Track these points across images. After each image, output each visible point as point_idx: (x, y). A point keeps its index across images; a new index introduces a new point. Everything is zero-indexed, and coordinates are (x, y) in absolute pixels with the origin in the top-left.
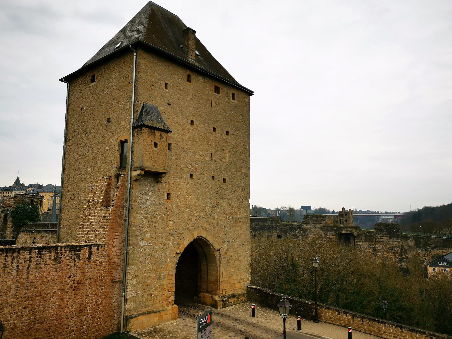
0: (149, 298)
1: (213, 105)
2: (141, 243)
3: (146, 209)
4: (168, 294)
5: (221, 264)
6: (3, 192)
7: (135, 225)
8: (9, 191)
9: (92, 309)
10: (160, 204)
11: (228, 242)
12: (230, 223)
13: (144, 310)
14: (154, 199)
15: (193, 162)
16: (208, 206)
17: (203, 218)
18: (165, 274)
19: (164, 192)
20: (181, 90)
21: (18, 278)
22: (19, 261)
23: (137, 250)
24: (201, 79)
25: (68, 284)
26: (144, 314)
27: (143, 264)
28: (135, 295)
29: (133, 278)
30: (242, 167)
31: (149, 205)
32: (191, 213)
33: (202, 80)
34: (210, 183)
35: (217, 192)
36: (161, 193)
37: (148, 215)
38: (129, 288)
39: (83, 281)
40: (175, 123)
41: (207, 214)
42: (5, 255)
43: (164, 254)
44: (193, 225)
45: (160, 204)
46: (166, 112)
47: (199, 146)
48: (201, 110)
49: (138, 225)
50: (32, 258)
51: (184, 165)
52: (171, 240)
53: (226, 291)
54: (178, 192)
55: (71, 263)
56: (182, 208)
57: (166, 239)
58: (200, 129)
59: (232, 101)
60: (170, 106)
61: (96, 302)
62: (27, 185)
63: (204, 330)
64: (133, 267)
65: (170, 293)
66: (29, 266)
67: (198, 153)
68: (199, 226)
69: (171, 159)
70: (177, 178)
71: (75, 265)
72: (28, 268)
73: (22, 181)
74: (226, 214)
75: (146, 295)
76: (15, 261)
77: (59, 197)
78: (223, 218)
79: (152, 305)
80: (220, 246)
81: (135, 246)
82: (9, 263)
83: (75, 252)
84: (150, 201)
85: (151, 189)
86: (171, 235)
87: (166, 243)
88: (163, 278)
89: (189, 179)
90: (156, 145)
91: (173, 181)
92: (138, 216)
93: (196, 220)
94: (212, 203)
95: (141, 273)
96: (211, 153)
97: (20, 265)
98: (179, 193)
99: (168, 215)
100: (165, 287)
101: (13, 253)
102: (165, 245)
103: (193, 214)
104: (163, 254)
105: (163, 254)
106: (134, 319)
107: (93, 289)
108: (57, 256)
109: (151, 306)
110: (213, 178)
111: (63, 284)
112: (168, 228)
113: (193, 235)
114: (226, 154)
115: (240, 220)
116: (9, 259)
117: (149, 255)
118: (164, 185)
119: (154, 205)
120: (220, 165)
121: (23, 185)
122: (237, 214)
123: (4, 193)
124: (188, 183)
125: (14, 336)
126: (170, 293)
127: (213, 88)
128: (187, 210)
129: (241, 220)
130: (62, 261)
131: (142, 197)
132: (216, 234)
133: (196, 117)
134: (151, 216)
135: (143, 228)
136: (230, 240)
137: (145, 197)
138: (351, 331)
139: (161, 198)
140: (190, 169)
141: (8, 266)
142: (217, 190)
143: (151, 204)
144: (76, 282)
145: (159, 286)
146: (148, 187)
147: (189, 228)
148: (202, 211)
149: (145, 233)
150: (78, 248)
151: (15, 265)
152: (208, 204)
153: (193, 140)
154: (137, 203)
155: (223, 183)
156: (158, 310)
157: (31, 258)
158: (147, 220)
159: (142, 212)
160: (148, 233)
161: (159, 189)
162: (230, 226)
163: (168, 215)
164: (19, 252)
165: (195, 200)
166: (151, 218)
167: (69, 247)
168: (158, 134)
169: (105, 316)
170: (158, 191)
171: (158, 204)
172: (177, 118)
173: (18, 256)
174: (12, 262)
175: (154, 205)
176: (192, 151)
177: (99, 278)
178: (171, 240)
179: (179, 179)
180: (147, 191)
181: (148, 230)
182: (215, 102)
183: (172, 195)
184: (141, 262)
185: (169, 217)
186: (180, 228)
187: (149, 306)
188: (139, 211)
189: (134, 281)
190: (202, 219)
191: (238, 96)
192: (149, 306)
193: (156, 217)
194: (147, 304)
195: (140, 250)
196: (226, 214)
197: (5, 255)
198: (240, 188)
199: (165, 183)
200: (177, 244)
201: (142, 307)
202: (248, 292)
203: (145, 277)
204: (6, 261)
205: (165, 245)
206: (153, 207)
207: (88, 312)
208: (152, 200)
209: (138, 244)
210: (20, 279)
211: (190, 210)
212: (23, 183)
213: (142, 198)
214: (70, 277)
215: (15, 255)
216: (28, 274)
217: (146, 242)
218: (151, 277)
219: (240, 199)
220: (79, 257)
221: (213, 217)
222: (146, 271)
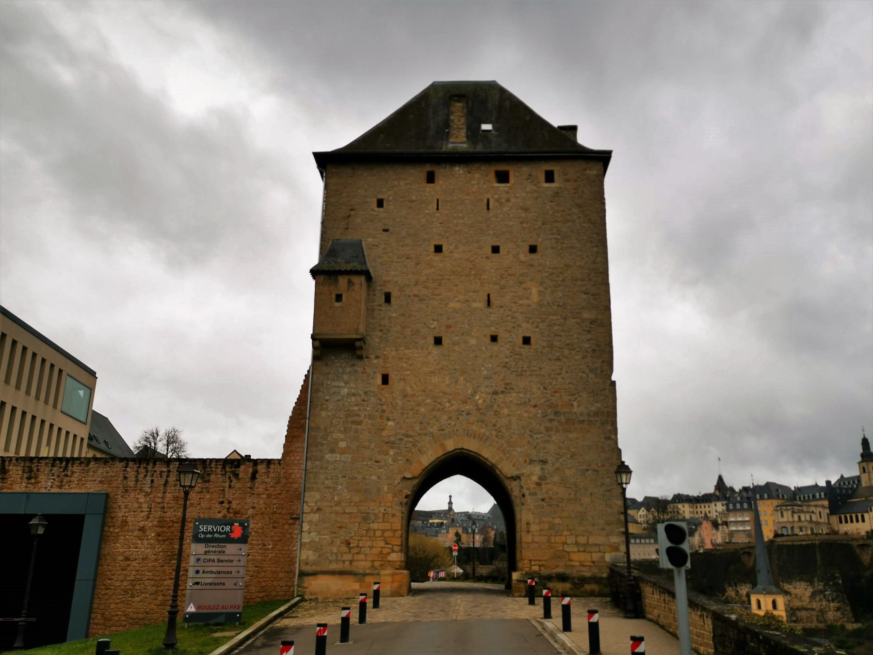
0: (344, 548)
1: (491, 207)
2: (328, 456)
3: (339, 403)
4: (385, 547)
5: (523, 507)
6: (695, 506)
7: (318, 428)
8: (701, 503)
9: (257, 555)
10: (366, 393)
11: (544, 462)
12: (549, 425)
13: (334, 567)
14: (354, 386)
15: (441, 315)
16: (482, 393)
17: (468, 414)
18: (377, 512)
19: (375, 373)
20: (412, 201)
21: (152, 496)
22: (153, 474)
23: (322, 468)
25: (219, 512)
26: (333, 573)
27: (331, 491)
28: (317, 540)
29: (312, 511)
30: (583, 308)
31: (344, 396)
32: (439, 406)
33: (461, 172)
34: (486, 349)
35: (504, 364)
36: (369, 375)
37: (342, 411)
38: (306, 527)
39: (242, 511)
40: (398, 258)
41: (480, 407)
42: (138, 465)
43: (376, 477)
44: (444, 427)
45: (366, 393)
46: (379, 243)
47: (456, 286)
48: (461, 221)
49: (322, 427)
50: (170, 471)
51: (420, 323)
52: (391, 453)
53: (543, 565)
54: (407, 370)
55: (225, 482)
56: (415, 399)
57: (379, 452)
58: (456, 255)
60: (388, 233)
61: (264, 545)
62: (737, 488)
63: (217, 544)
64: (312, 493)
65: (391, 546)
66: (167, 482)
67: (454, 297)
68: (457, 430)
69: (390, 318)
70: (402, 348)
71: (230, 486)
72: (165, 485)
73: (728, 482)
74: (535, 406)
75: (338, 542)
76: (149, 474)
77: (789, 508)
78: (526, 415)
79: (351, 562)
80: (518, 469)
81: (317, 461)
82: (141, 476)
83: (231, 468)
84: (346, 390)
85: (348, 369)
86: (392, 444)
87: (379, 458)
88: (373, 518)
89: (431, 347)
91: (394, 353)
92: (324, 414)
93: (450, 418)
94: (492, 386)
95: (328, 504)
96: (489, 295)
97: (155, 480)
98: (409, 373)
99: (383, 411)
100: (378, 533)
101: (148, 464)
102: (377, 462)
103: (443, 409)
104: (374, 478)
105: (374, 478)
106: (311, 578)
107: (260, 524)
108: (205, 472)
109: (347, 563)
110: (494, 339)
111: (212, 511)
112: (385, 433)
113: (443, 446)
114: (530, 289)
115: (581, 418)
116: (142, 470)
117: (344, 477)
118: (376, 361)
119: (354, 395)
120: (514, 312)
121: (732, 489)
122: (572, 405)
123: (697, 507)
124: (430, 353)
125: (144, 569)
126: (391, 546)
127: (492, 176)
128: (428, 401)
129: (586, 418)
130: (211, 480)
131: (331, 383)
132: (505, 445)
133: (448, 238)
134: (348, 413)
135: (333, 432)
136: (550, 459)
137: (336, 384)
138: (595, 618)
139: (369, 384)
140: (434, 328)
141: (140, 479)
142: (507, 360)
143: (348, 395)
144: (231, 511)
145: (365, 532)
146: (341, 367)
147: (432, 433)
148: (465, 402)
149: (336, 442)
150: (236, 463)
151: (149, 479)
152: (483, 389)
153: (440, 278)
154: (320, 394)
155: (522, 345)
156: (361, 571)
157: (169, 471)
158: (339, 420)
159: (331, 407)
160: (342, 440)
161: (364, 369)
162: (548, 429)
163: (383, 411)
164: (154, 464)
165: (447, 382)
166: (347, 416)
167: (222, 461)
168: (343, 281)
169: (279, 569)
170: (363, 373)
171: (362, 393)
172: (402, 248)
173: (153, 468)
174: (146, 476)
175: (354, 395)
176: (438, 298)
177: (268, 509)
178: (391, 453)
179: (409, 349)
180: (341, 373)
181: (342, 436)
182: (497, 200)
183: (392, 377)
184: (328, 488)
185: (385, 414)
186: (411, 433)
187: (344, 562)
188: (325, 406)
189: (316, 517)
190: (465, 415)
191: (563, 172)
192: (344, 562)
193: (358, 415)
194: (339, 559)
195: (326, 468)
196: (535, 406)
197: (138, 465)
198: (578, 351)
199: (377, 357)
200: (405, 460)
201: (331, 562)
202: (610, 577)
203: (337, 513)
204: (138, 474)
205: (377, 462)
206: (353, 399)
207: (250, 557)
208: (350, 388)
209: (323, 457)
210: (154, 498)
211: (436, 402)
212: (731, 485)
213: (329, 385)
214: (222, 503)
215: (150, 467)
216: (165, 493)
217: (338, 455)
218: (349, 513)
219: (580, 374)
220: (236, 476)
221: (496, 411)
222: (338, 504)
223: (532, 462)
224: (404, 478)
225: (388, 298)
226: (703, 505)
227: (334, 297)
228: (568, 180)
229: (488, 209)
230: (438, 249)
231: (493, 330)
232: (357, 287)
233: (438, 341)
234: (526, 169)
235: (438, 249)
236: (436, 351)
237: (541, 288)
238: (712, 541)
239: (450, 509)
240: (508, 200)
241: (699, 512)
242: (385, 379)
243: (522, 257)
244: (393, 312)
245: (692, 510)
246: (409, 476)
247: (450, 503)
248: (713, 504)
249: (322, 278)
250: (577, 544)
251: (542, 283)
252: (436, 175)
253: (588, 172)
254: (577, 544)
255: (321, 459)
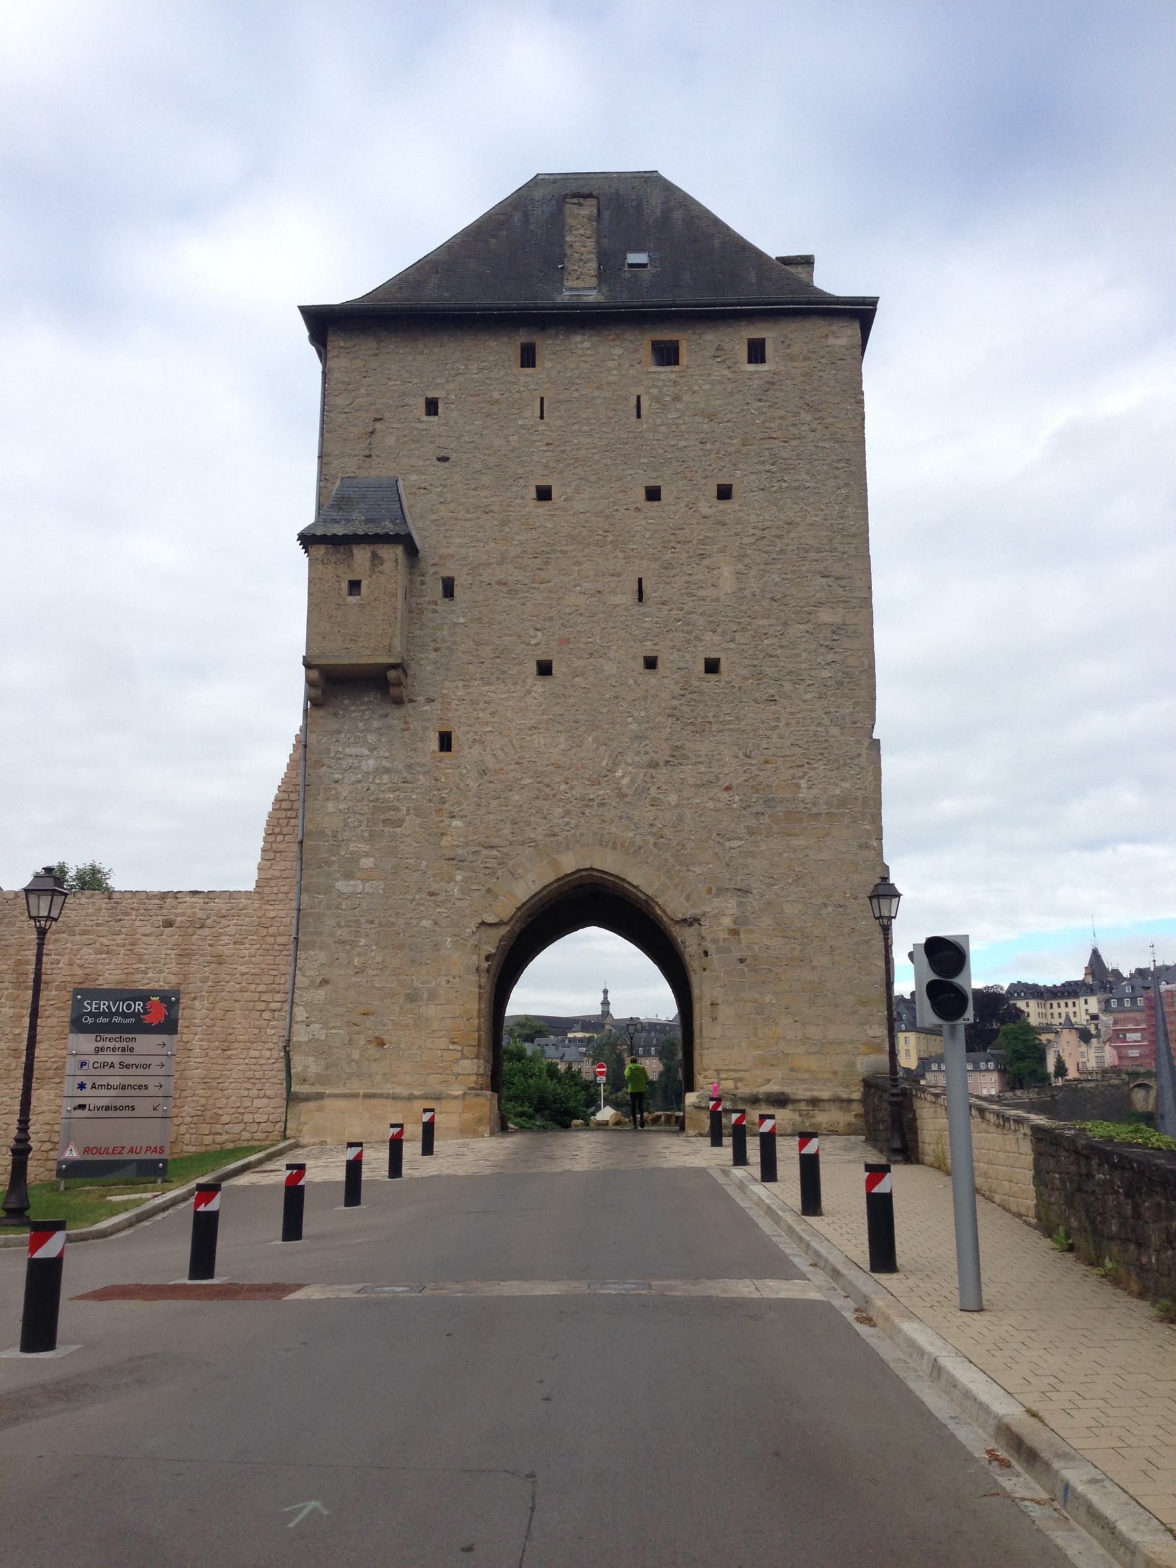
2: (340, 885)
11: (744, 891)
24: (583, 344)
59: (752, 367)
74: (728, 788)
78: (711, 805)
90: (355, 586)
92: (331, 806)
113: (555, 864)
119: (387, 771)
160: (367, 855)
168: (362, 555)
175: (387, 771)
182: (656, 399)
199: (430, 701)
223: (721, 891)
224: (483, 923)
225: (449, 589)
226: (1062, 1003)
227: (345, 586)
228: (791, 358)
229: (639, 416)
230: (544, 494)
231: (649, 649)
232: (388, 566)
233: (545, 669)
234: (711, 338)
235: (544, 494)
236: (540, 686)
237: (740, 567)
238: (1078, 1064)
239: (606, 1014)
240: (677, 399)
241: (1056, 1015)
242: (446, 741)
243: (704, 508)
244: (458, 612)
245: (1043, 1011)
246: (491, 919)
247: (606, 1003)
248: (1082, 1000)
249: (320, 550)
250: (805, 1039)
251: (741, 557)
252: (537, 351)
253: (831, 341)
254: (805, 1039)
255: (329, 889)
